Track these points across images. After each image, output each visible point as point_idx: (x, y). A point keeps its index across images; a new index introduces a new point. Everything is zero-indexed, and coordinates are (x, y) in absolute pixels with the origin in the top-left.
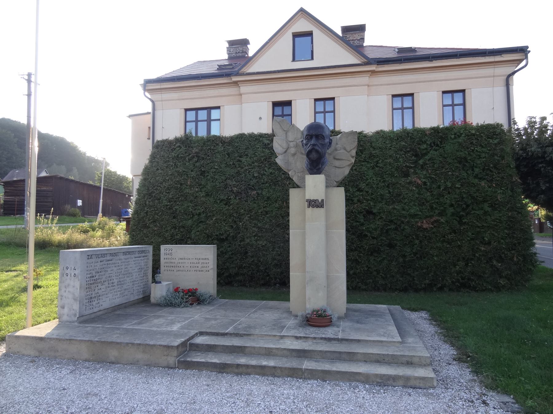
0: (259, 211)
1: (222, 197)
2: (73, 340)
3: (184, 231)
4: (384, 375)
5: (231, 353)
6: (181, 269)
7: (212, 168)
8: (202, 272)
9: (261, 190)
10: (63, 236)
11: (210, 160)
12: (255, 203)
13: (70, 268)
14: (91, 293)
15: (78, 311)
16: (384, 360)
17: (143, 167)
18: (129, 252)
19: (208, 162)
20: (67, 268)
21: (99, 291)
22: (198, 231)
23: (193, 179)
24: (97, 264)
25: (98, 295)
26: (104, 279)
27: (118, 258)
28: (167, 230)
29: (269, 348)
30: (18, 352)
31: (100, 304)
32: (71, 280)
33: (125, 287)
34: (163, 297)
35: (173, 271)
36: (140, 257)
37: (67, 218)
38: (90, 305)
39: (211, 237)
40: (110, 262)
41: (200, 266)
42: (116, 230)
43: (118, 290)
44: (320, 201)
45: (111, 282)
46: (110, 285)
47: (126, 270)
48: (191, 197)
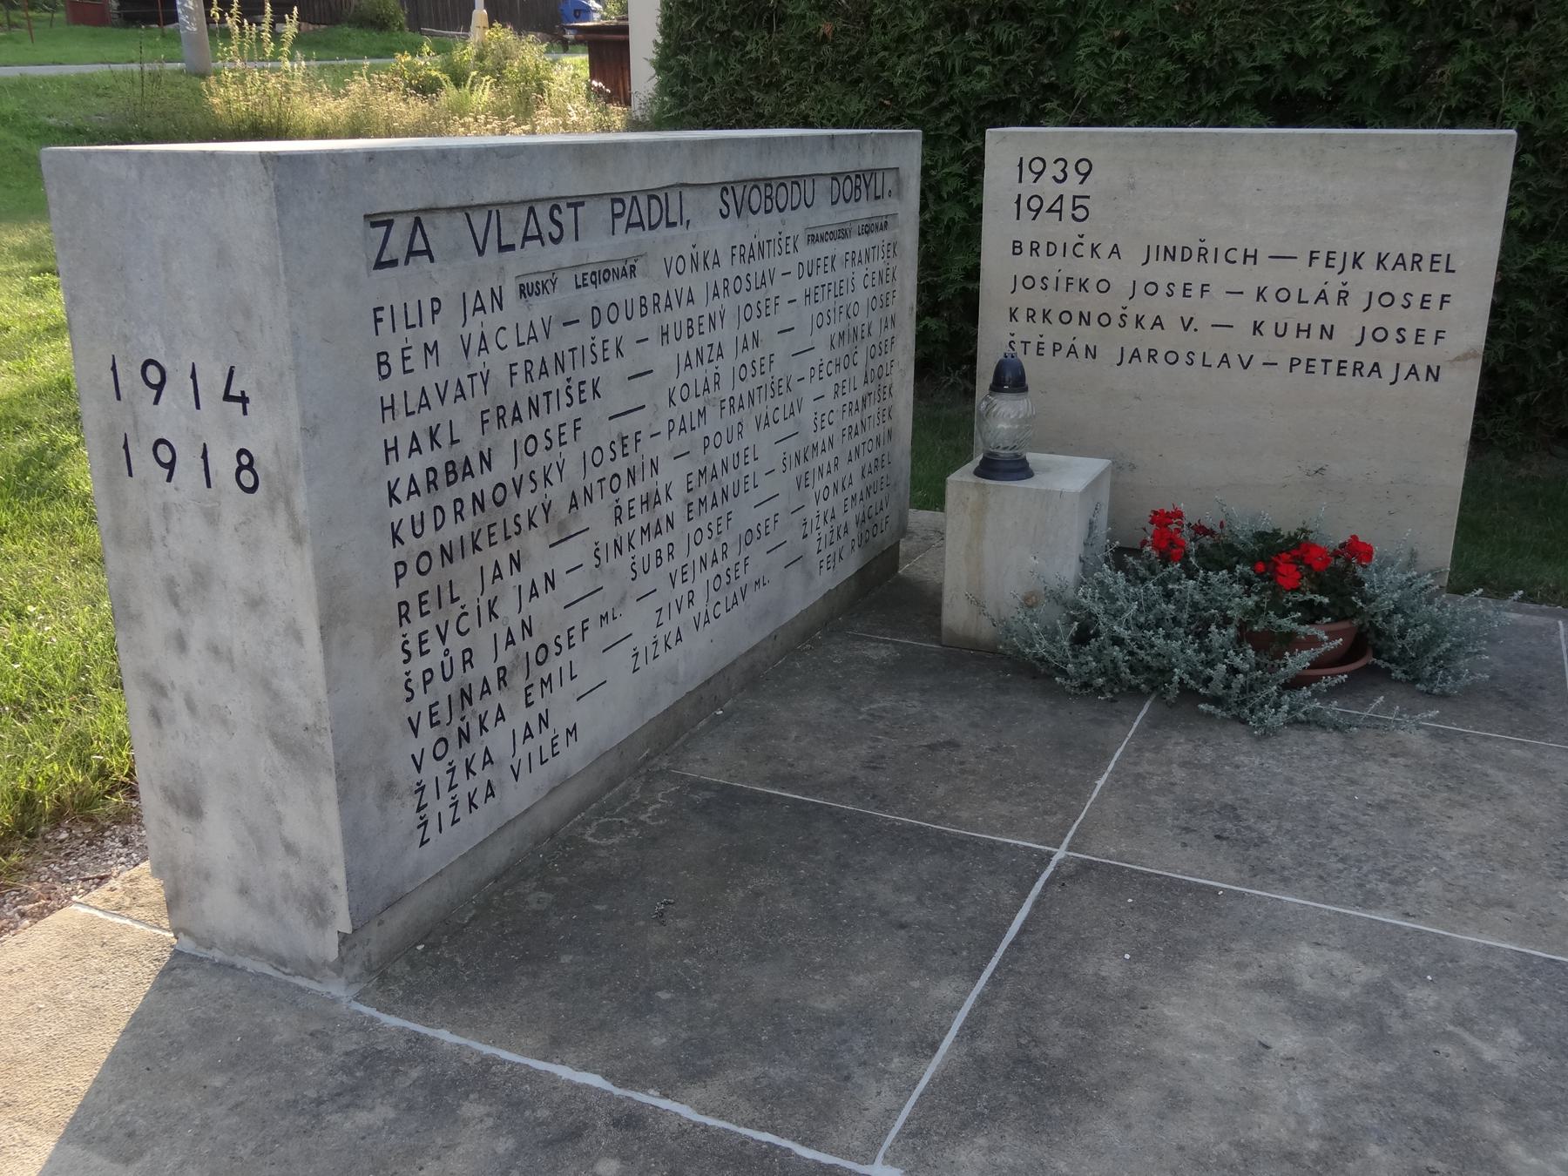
3: (1017, 40)
6: (1163, 341)
10: (331, 104)
13: (178, 386)
14: (456, 643)
15: (338, 875)
18: (768, 182)
21: (543, 608)
22: (1123, 41)
24: (493, 319)
25: (530, 645)
26: (574, 476)
27: (678, 241)
28: (902, 38)
31: (559, 723)
33: (746, 514)
34: (1056, 597)
35: (1091, 352)
36: (843, 234)
37: (357, 37)
38: (461, 771)
39: (1216, 85)
40: (615, 291)
41: (1349, 321)
42: (551, 80)
43: (696, 553)
45: (639, 490)
46: (628, 526)
47: (746, 358)
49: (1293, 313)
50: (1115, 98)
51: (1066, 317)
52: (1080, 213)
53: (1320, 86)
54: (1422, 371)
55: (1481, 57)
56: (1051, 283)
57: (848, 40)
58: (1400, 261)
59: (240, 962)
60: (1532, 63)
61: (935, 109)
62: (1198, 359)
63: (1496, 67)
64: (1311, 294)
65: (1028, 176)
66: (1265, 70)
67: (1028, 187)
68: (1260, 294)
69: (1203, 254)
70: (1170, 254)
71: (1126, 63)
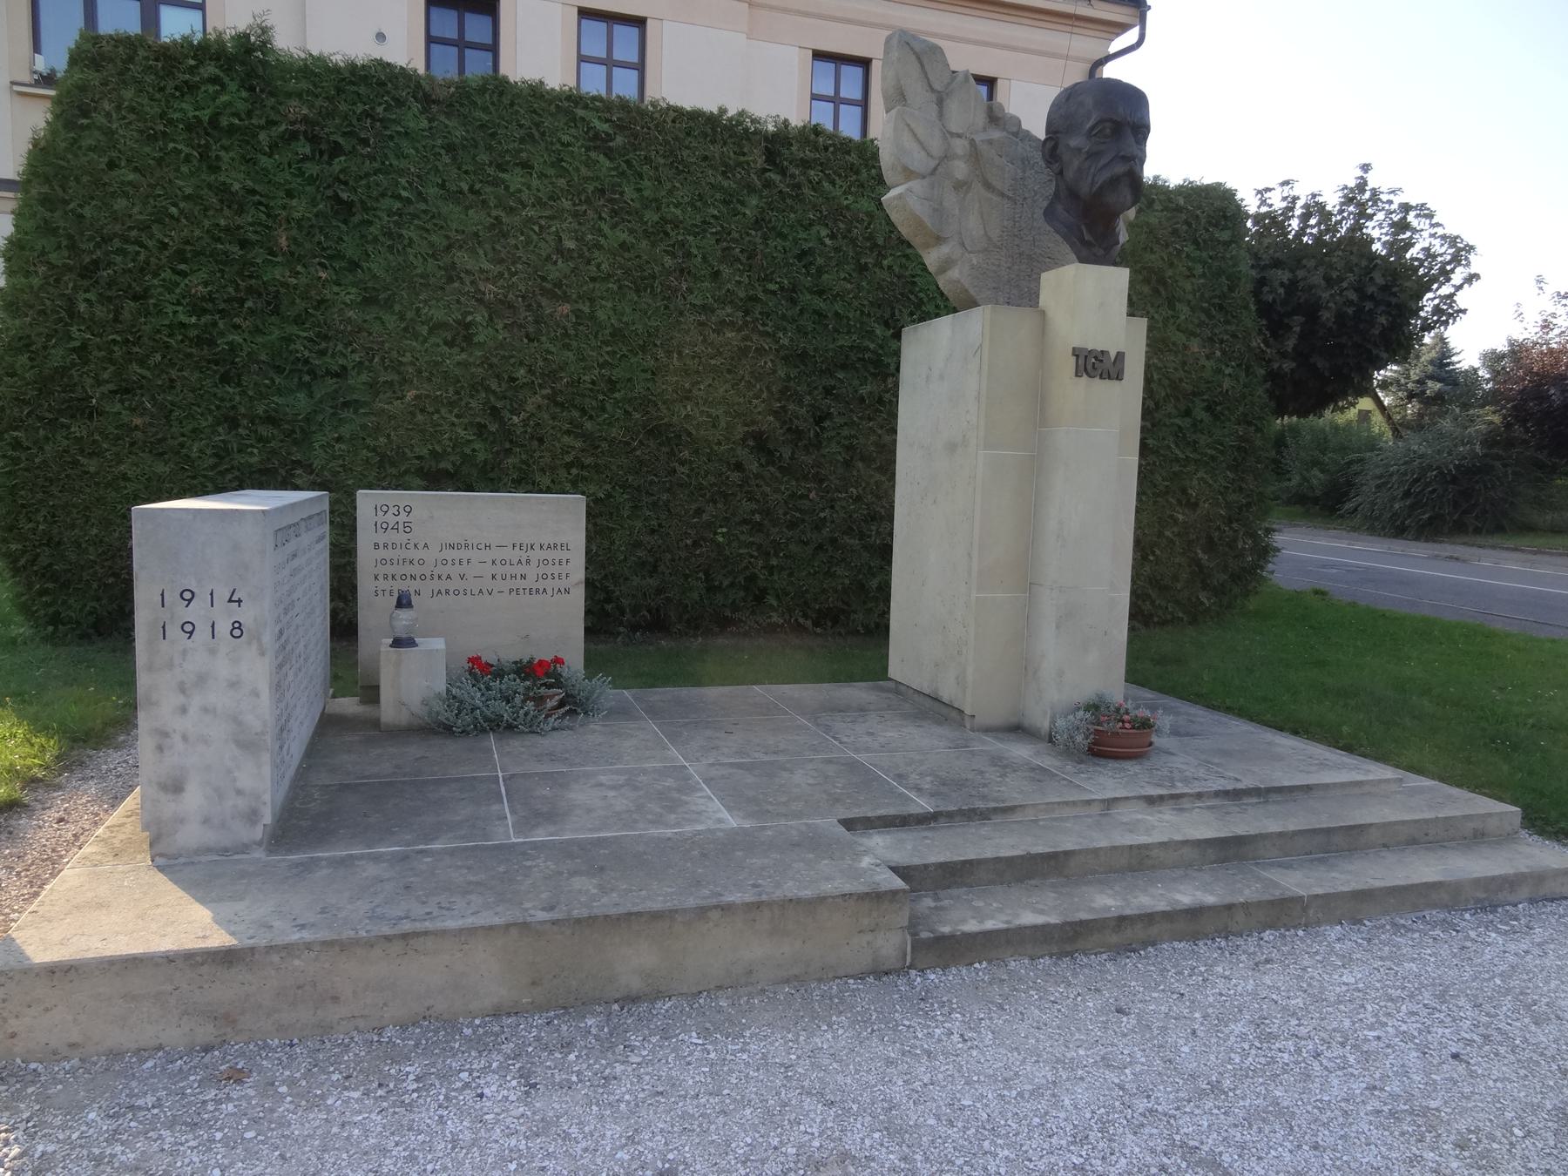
0: (587, 378)
1: (438, 314)
2: (426, 933)
4: (1493, 878)
5: (1020, 880)
6: (451, 585)
7: (383, 195)
8: (539, 597)
9: (588, 304)
11: (372, 158)
12: (567, 347)
16: (1427, 835)
17: (25, 147)
19: (368, 166)
20: (188, 597)
22: (338, 440)
23: (300, 228)
29: (1140, 847)
30: (72, 1046)
32: (213, 652)
44: (1113, 355)
48: (298, 301)
49: (508, 569)
50: (338, 469)
51: (404, 577)
52: (408, 530)
53: (450, 467)
54: (563, 590)
55: (524, 457)
56: (395, 562)
57: (154, 430)
58: (549, 547)
59: (197, 859)
60: (548, 460)
61: (220, 472)
62: (469, 592)
63: (531, 461)
64: (515, 561)
65: (380, 513)
66: (419, 458)
67: (381, 518)
68: (493, 562)
69: (467, 546)
70: (452, 547)
71: (343, 451)
